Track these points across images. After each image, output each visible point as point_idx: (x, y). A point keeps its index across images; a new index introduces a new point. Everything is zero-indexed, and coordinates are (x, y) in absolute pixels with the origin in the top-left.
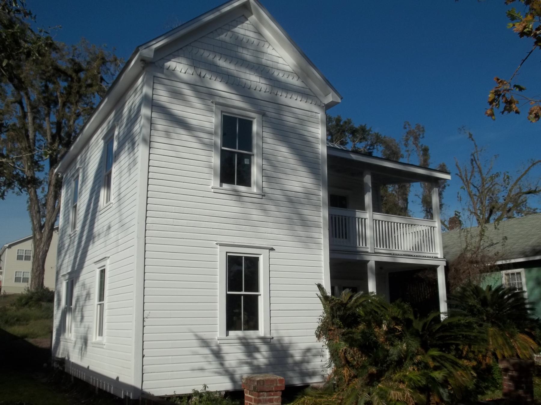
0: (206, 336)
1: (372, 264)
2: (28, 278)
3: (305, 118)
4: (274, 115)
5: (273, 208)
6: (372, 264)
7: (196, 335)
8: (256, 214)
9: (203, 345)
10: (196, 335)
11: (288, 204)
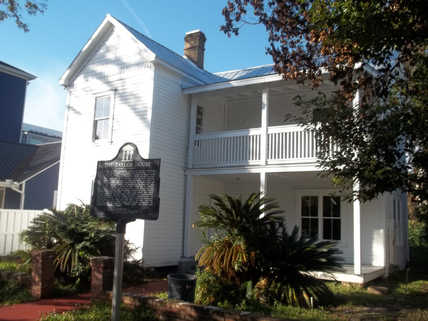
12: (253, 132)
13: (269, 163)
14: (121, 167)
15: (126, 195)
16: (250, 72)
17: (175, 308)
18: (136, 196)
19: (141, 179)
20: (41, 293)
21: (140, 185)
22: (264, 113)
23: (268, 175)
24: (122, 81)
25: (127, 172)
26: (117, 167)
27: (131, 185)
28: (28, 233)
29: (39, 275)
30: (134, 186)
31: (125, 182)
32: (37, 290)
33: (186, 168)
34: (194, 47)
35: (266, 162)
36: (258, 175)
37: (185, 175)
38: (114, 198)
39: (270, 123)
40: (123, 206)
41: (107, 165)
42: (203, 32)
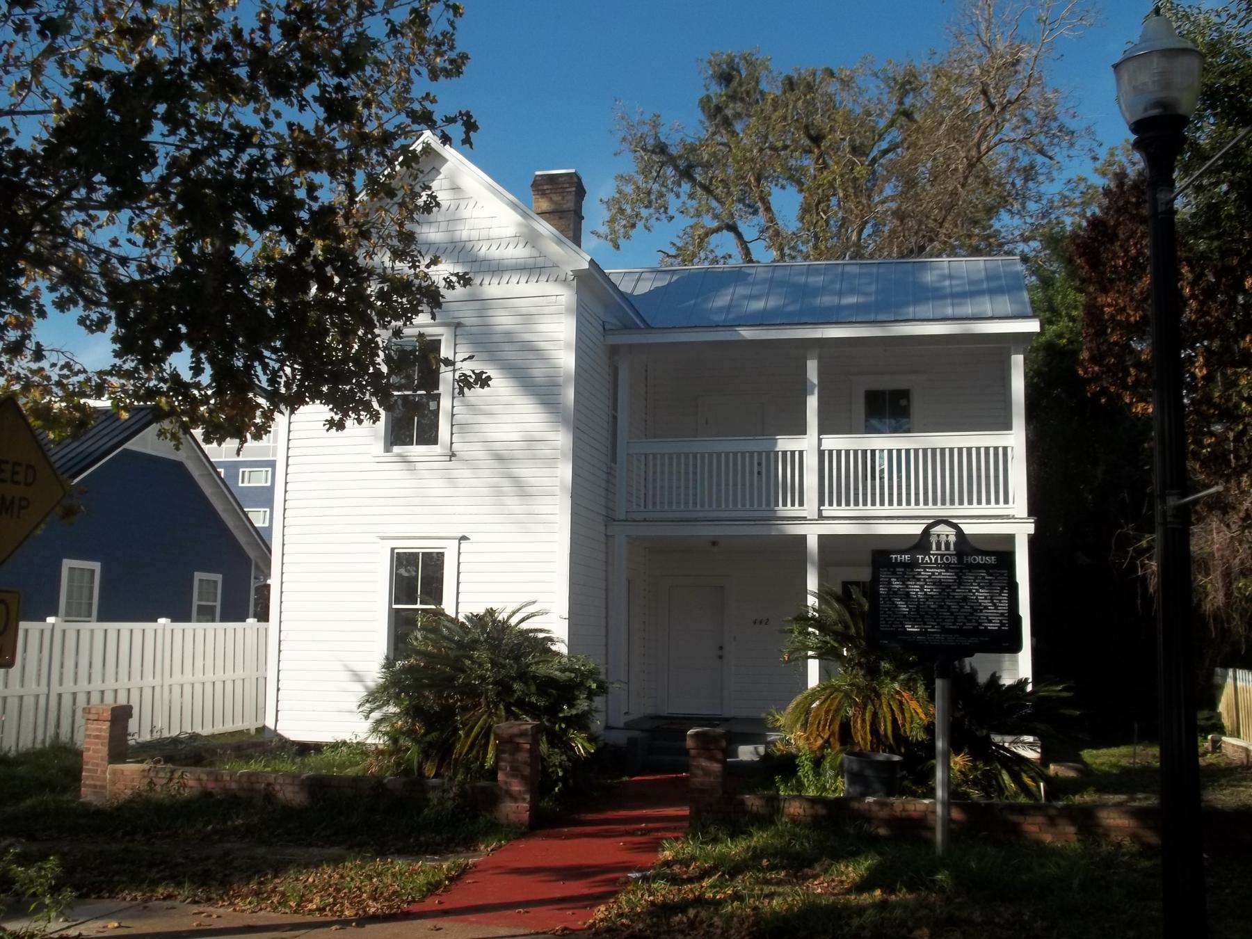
0: (357, 667)
1: (812, 544)
2: (1002, 553)
3: (533, 310)
4: (474, 321)
5: (466, 473)
6: (812, 544)
7: (345, 666)
8: (436, 486)
9: (354, 679)
10: (345, 666)
11: (494, 463)
12: (785, 444)
13: (825, 514)
14: (931, 563)
15: (948, 611)
16: (675, 278)
17: (915, 810)
18: (971, 614)
19: (979, 585)
20: (530, 816)
21: (981, 595)
22: (812, 402)
23: (821, 538)
24: (477, 305)
25: (947, 571)
26: (922, 563)
27: (959, 593)
28: (383, 689)
29: (524, 778)
30: (965, 597)
31: (943, 590)
32: (516, 809)
33: (609, 520)
34: (563, 212)
35: (820, 511)
36: (804, 537)
37: (606, 535)
38: (922, 617)
39: (824, 429)
40: (944, 630)
41: (896, 558)
42: (581, 174)
